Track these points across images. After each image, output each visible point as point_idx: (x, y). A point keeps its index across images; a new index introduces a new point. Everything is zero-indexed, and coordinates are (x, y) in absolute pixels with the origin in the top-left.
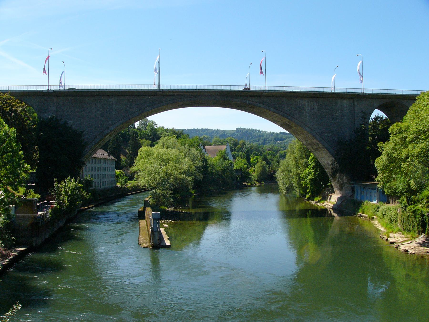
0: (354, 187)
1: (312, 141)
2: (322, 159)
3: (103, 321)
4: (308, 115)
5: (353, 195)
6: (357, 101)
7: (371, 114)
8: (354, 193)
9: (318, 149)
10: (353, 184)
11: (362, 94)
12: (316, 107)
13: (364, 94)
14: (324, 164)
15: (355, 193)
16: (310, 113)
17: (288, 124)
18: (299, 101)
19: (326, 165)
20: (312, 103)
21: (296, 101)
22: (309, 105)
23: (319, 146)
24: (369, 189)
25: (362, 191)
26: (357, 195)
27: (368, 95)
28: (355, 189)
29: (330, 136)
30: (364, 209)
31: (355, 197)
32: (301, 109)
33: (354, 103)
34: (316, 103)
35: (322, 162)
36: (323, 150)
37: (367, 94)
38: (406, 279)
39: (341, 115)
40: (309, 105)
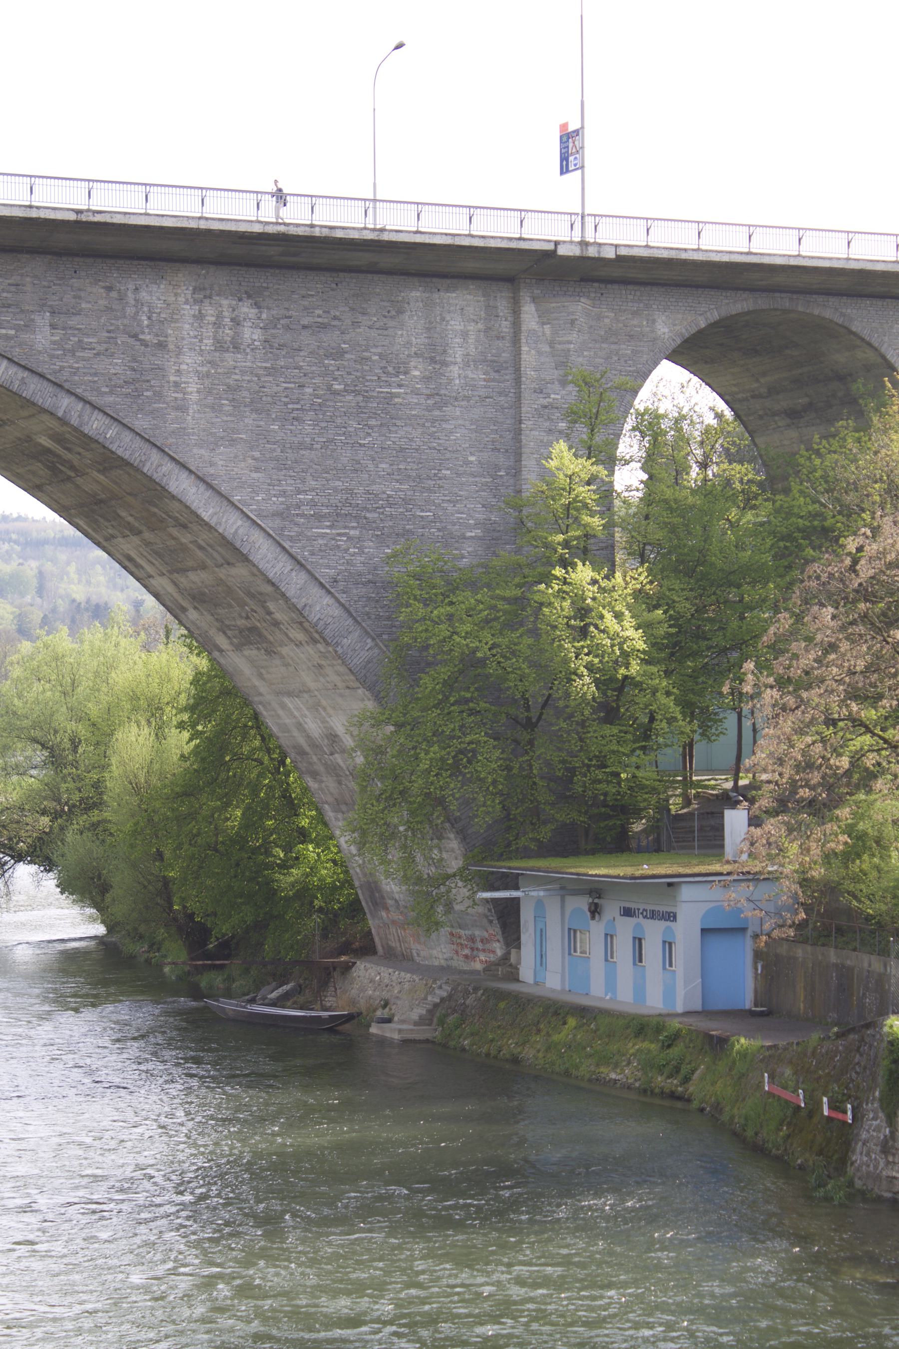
0: (516, 902)
1: (222, 573)
2: (283, 706)
3: (600, 1335)
4: (192, 388)
5: (506, 957)
6: (534, 300)
7: (635, 392)
8: (519, 947)
9: (260, 635)
10: (511, 881)
11: (576, 251)
12: (251, 334)
13: (592, 252)
14: (302, 741)
15: (524, 938)
16: (208, 375)
17: (48, 451)
18: (131, 286)
19: (314, 745)
20: (225, 302)
21: (109, 289)
22: (200, 317)
23: (270, 613)
24: (628, 913)
25: (572, 932)
26: (542, 957)
27: (620, 259)
28: (527, 915)
29: (350, 538)
30: (185, 709)
31: (526, 973)
32: (144, 344)
33: (516, 312)
34: (257, 305)
35: (285, 729)
36: (299, 644)
37: (610, 254)
38: (684, 701)
39: (429, 396)
40: (200, 317)
